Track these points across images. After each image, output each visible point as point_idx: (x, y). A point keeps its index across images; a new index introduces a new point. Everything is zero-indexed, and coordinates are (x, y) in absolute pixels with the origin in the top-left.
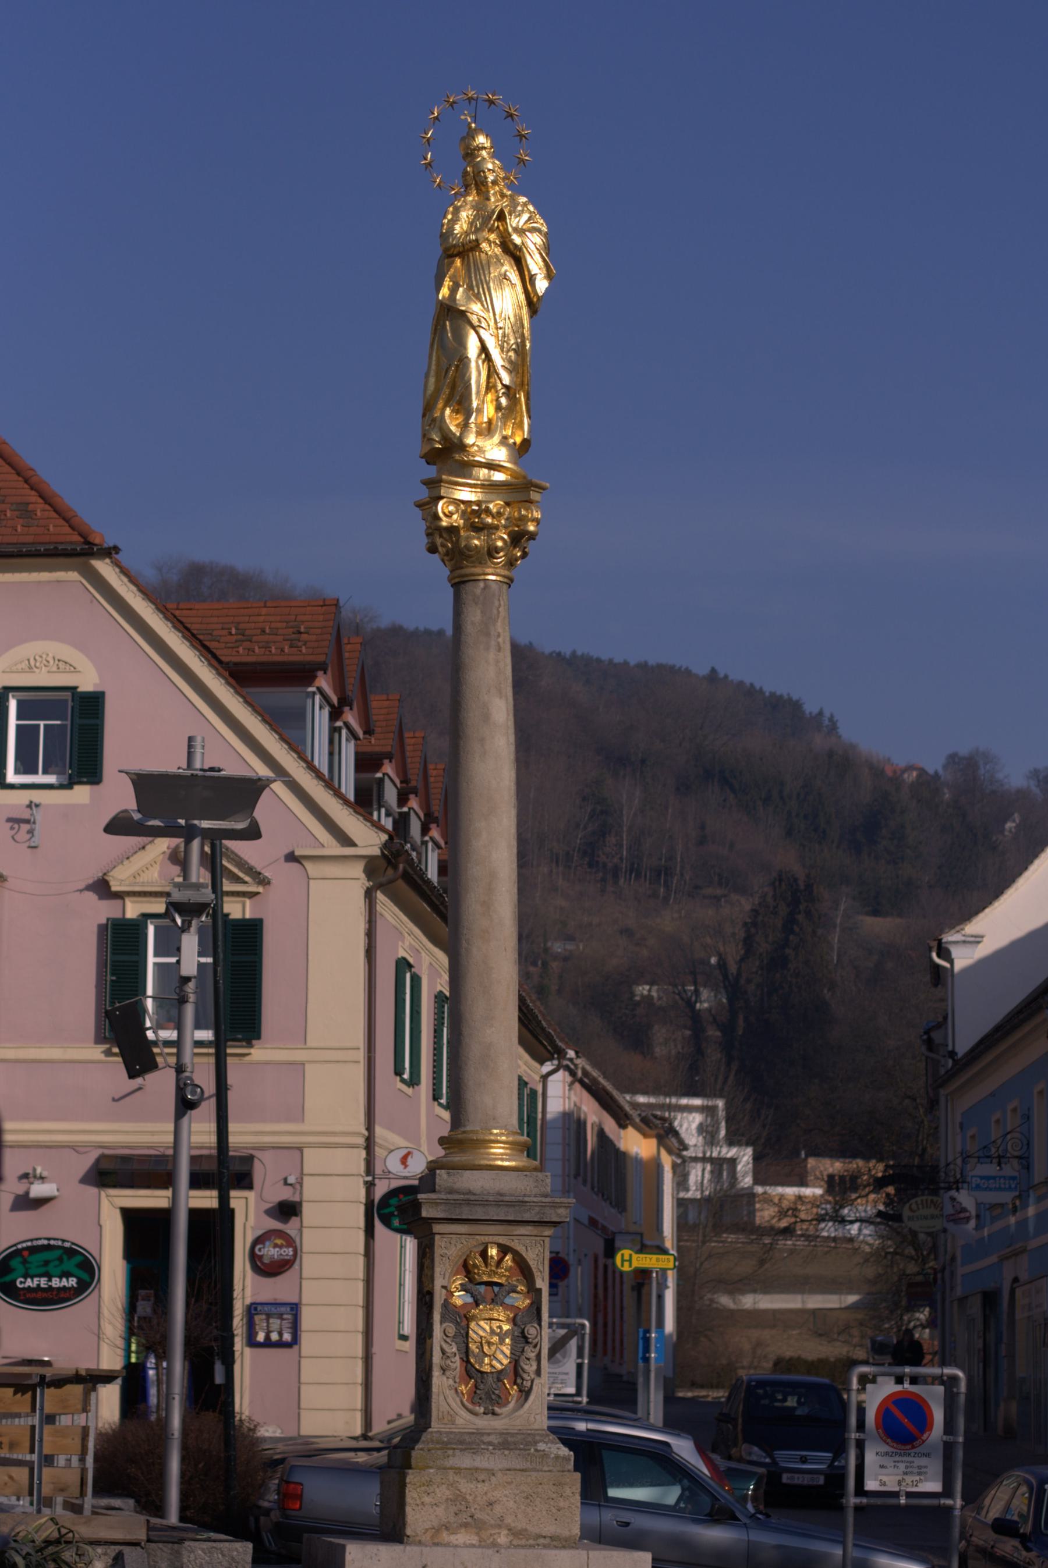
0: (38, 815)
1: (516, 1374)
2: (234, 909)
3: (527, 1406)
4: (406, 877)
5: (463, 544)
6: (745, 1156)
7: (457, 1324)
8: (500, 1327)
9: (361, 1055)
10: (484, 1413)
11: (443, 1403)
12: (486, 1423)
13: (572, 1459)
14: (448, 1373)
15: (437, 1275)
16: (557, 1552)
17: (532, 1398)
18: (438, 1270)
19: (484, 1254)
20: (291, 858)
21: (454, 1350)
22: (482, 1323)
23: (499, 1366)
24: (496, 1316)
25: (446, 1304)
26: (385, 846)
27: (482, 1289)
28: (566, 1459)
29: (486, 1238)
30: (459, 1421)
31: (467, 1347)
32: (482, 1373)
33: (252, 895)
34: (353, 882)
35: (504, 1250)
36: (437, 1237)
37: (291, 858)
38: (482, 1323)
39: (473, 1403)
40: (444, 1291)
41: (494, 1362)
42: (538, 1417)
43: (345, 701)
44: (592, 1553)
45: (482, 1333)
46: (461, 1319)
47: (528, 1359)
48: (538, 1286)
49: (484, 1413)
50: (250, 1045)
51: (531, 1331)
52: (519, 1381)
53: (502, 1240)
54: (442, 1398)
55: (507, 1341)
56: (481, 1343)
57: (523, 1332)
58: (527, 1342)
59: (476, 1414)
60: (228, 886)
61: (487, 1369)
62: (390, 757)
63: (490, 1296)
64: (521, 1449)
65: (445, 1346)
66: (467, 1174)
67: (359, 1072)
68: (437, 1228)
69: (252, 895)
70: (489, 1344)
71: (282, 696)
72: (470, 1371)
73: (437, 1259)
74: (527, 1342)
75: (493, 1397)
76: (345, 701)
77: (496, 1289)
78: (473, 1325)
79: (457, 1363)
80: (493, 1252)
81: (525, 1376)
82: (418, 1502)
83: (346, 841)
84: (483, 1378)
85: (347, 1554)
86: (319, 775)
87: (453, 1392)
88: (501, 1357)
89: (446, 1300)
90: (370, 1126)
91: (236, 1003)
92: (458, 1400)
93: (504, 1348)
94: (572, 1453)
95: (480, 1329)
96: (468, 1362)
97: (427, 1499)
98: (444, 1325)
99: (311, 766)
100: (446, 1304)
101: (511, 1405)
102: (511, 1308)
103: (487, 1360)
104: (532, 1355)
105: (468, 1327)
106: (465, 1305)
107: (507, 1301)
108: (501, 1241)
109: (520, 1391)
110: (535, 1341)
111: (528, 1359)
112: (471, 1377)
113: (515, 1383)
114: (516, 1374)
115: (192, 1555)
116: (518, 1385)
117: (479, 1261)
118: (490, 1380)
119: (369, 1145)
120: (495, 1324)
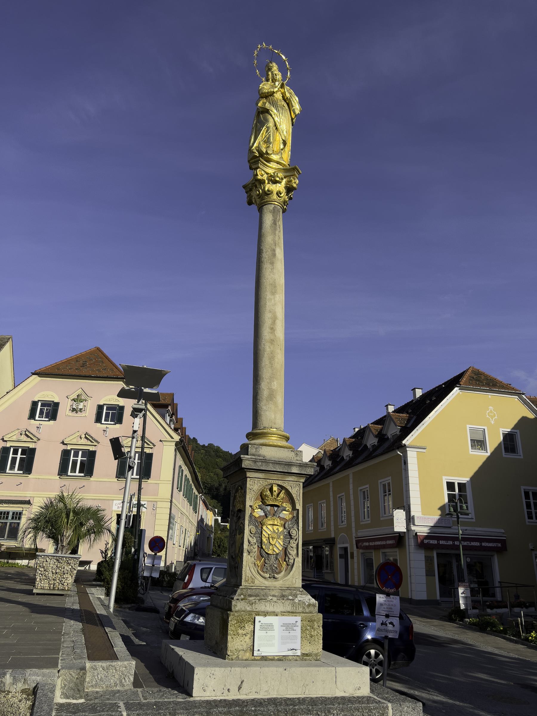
0: (108, 430)
1: (286, 554)
2: (147, 451)
3: (291, 573)
4: (183, 447)
5: (266, 189)
6: (219, 519)
7: (256, 526)
8: (278, 529)
9: (171, 482)
10: (269, 577)
11: (248, 572)
12: (270, 583)
13: (317, 605)
14: (251, 554)
15: (247, 499)
16: (317, 669)
17: (294, 569)
18: (248, 497)
19: (271, 490)
20: (161, 441)
21: (255, 541)
22: (269, 527)
23: (277, 552)
24: (276, 523)
25: (251, 516)
26: (180, 439)
27: (269, 508)
28: (314, 605)
29: (272, 481)
30: (257, 582)
31: (262, 540)
32: (268, 554)
33: (151, 448)
34: (173, 447)
35: (281, 487)
36: (248, 479)
37: (161, 441)
38: (269, 527)
39: (263, 572)
40: (250, 508)
41: (275, 549)
42: (297, 580)
43: (173, 414)
44: (339, 669)
45: (269, 533)
46: (259, 524)
47: (292, 547)
48: (297, 508)
49: (269, 577)
50: (148, 479)
51: (294, 532)
52: (287, 559)
53: (280, 483)
54: (248, 568)
55: (282, 537)
56: (269, 538)
57: (289, 533)
58: (291, 538)
59: (265, 578)
60: (146, 445)
61: (270, 552)
62: (180, 428)
63: (272, 512)
64: (290, 600)
65: (250, 539)
66: (264, 448)
67: (171, 485)
68: (249, 474)
69: (151, 448)
70: (272, 538)
71: (163, 410)
72: (262, 554)
73: (248, 491)
74: (291, 538)
75: (274, 568)
76: (173, 414)
77: (276, 508)
78: (264, 528)
79: (256, 549)
80: (275, 488)
81: (290, 557)
82: (235, 633)
83: (172, 438)
84: (268, 557)
85: (195, 675)
86: (167, 424)
87: (253, 565)
88: (278, 546)
89: (251, 513)
90: (172, 498)
91: (145, 471)
92: (255, 569)
93: (279, 541)
94: (317, 602)
95: (267, 530)
96: (262, 548)
97: (240, 631)
98: (250, 527)
99: (166, 423)
100: (251, 516)
101: (283, 573)
102: (281, 519)
103: (271, 547)
104: (294, 546)
105: (262, 528)
106: (260, 517)
107: (281, 515)
108: (279, 483)
109: (288, 565)
110: (295, 538)
111: (292, 547)
112: (262, 557)
113: (285, 561)
114: (286, 554)
115: (95, 672)
116: (286, 562)
117: (268, 493)
118: (273, 558)
119: (171, 502)
120: (275, 528)
